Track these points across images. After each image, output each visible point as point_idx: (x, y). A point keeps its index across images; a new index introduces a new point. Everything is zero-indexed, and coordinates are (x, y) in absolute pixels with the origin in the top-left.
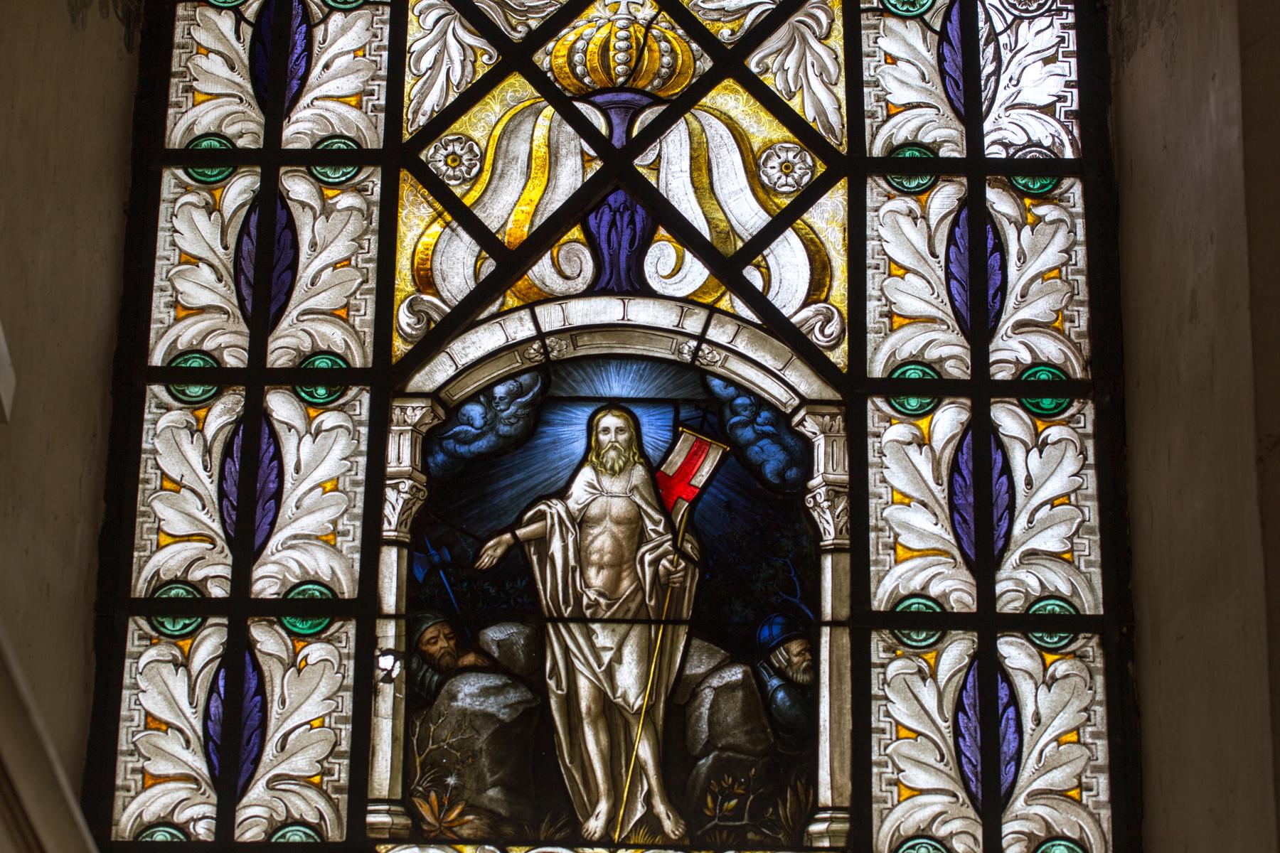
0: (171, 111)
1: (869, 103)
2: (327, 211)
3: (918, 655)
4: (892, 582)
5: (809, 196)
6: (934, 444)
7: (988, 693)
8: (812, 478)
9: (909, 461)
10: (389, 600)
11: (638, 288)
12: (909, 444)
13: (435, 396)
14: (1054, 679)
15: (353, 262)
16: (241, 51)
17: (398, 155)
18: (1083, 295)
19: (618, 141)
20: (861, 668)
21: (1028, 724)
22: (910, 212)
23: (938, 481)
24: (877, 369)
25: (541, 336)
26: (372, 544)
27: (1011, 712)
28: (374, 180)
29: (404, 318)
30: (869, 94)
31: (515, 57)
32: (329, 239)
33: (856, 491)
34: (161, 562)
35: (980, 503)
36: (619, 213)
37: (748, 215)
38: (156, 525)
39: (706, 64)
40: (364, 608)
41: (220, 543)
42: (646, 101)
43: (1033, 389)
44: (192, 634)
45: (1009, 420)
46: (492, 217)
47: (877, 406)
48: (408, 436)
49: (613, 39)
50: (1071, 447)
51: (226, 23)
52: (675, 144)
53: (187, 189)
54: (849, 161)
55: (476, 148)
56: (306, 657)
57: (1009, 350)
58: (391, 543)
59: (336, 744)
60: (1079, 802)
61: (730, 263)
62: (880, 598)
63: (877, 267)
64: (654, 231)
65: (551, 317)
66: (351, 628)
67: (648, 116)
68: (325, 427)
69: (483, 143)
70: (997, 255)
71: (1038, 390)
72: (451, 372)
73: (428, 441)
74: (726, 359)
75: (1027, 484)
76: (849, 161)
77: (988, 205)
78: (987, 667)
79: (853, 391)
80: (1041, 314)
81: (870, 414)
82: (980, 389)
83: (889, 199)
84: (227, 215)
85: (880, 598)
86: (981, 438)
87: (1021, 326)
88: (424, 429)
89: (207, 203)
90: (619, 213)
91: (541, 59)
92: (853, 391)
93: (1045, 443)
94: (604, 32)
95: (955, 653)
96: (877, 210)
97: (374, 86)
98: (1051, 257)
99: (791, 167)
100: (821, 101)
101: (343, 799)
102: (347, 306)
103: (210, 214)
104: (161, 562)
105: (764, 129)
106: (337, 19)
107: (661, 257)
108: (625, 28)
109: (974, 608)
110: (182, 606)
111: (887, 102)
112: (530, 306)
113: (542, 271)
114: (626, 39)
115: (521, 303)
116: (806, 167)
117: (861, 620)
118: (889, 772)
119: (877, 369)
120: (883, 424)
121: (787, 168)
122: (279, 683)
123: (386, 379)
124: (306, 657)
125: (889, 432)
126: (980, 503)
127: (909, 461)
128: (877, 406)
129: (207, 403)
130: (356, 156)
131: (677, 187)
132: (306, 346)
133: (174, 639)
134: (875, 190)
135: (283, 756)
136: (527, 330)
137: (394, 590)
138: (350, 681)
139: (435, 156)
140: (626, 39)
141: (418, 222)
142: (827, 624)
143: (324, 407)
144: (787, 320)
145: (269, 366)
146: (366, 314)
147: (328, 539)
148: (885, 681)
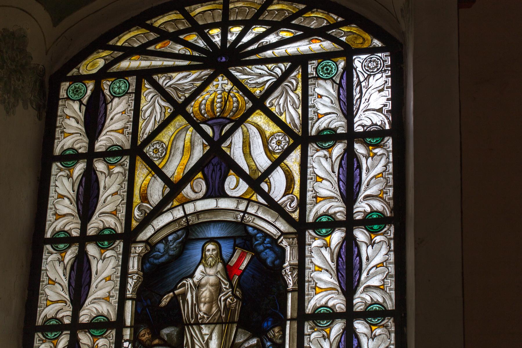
3: (323, 330)
4: (314, 302)
5: (286, 153)
7: (350, 249)
8: (285, 263)
9: (321, 254)
10: (128, 321)
12: (322, 247)
16: (81, 116)
18: (391, 183)
19: (216, 139)
20: (301, 335)
22: (325, 156)
24: (310, 218)
25: (186, 216)
28: (126, 160)
31: (179, 109)
32: (111, 183)
33: (301, 268)
34: (47, 312)
36: (216, 166)
40: (118, 324)
41: (69, 303)
44: (57, 338)
49: (216, 99)
52: (237, 138)
56: (97, 344)
62: (309, 308)
63: (312, 179)
64: (228, 172)
65: (190, 208)
66: (114, 332)
68: (107, 256)
69: (167, 143)
71: (371, 222)
73: (144, 259)
74: (254, 219)
75: (367, 260)
76: (302, 138)
77: (355, 150)
79: (301, 228)
81: (307, 237)
83: (317, 151)
84: (74, 179)
85: (309, 308)
86: (350, 242)
89: (68, 175)
90: (216, 166)
91: (189, 109)
93: (374, 243)
96: (312, 156)
98: (379, 168)
100: (292, 115)
102: (116, 210)
103: (69, 179)
105: (270, 128)
106: (116, 100)
107: (231, 181)
108: (221, 94)
109: (345, 310)
111: (318, 113)
112: (182, 205)
113: (187, 191)
115: (179, 204)
116: (286, 141)
117: (302, 317)
118: (312, 284)
119: (310, 218)
120: (312, 240)
121: (279, 143)
123: (129, 236)
124: (97, 344)
127: (321, 254)
128: (310, 233)
130: (120, 152)
131: (237, 154)
134: (311, 149)
136: (181, 214)
139: (149, 150)
140: (221, 98)
141: (142, 175)
146: (122, 214)
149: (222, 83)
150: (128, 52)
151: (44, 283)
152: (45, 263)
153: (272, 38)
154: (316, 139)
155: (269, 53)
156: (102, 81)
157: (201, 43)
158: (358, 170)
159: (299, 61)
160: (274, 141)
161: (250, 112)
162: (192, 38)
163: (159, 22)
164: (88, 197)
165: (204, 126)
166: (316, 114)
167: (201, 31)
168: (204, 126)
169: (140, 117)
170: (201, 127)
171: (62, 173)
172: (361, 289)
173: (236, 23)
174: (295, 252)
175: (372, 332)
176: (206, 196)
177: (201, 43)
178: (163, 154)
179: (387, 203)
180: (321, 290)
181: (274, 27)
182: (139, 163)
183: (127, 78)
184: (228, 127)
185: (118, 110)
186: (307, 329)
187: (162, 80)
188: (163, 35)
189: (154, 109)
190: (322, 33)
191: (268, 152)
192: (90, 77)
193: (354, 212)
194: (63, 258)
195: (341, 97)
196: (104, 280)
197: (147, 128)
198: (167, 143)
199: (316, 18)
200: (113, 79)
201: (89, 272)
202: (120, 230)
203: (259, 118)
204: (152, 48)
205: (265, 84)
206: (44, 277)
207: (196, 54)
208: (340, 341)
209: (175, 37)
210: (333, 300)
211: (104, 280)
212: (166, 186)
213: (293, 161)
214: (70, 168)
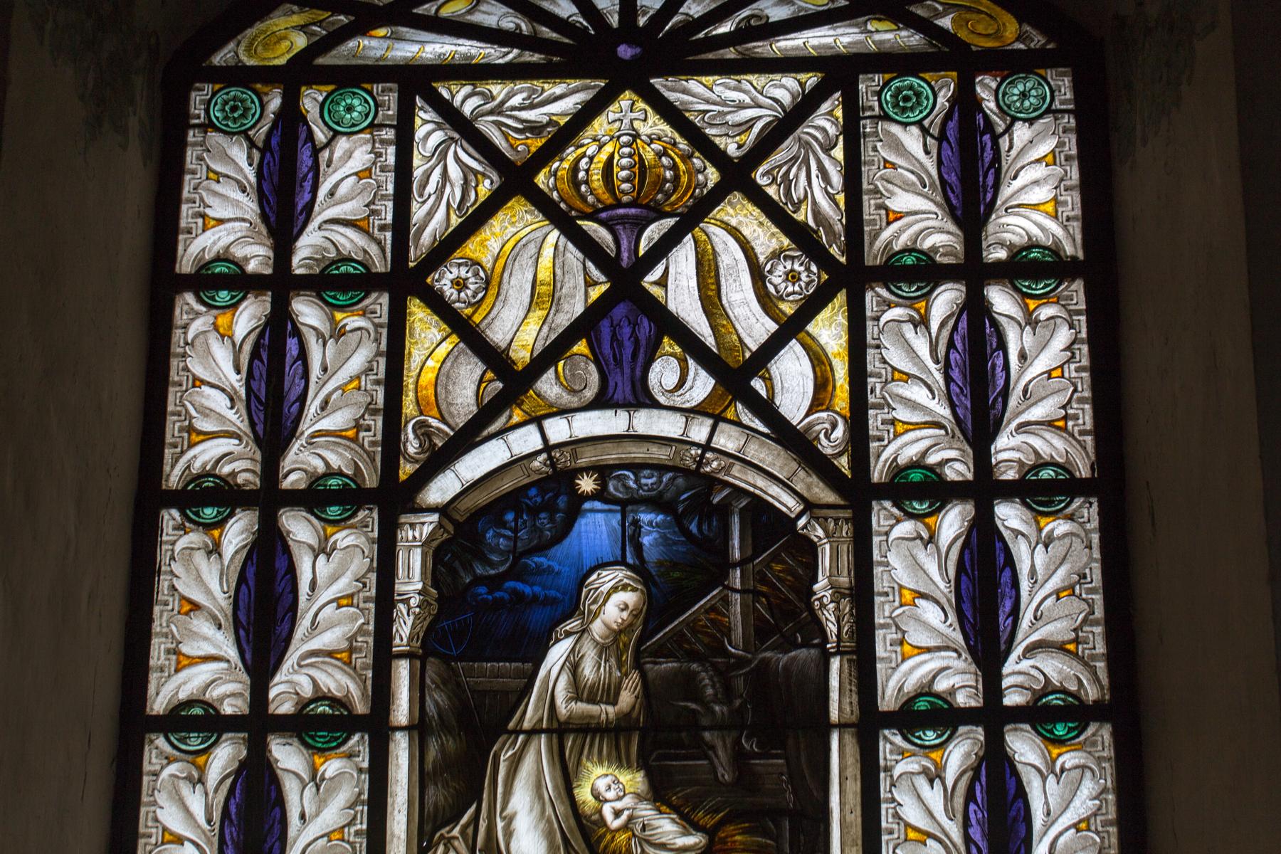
0: (181, 237)
1: (873, 364)
2: (339, 333)
4: (898, 680)
5: (812, 306)
6: (941, 544)
8: (817, 582)
9: (915, 561)
10: (402, 711)
11: (642, 399)
13: (444, 510)
15: (355, 601)
17: (405, 279)
18: (1099, 613)
20: (870, 771)
21: (1025, 585)
22: (924, 771)
24: (878, 473)
25: (548, 448)
26: (383, 656)
27: (1007, 573)
28: (381, 303)
29: (412, 446)
30: (869, 203)
31: (516, 180)
32: (339, 361)
33: (861, 593)
35: (984, 589)
36: (622, 331)
37: (755, 327)
38: (187, 423)
39: (712, 175)
40: (377, 726)
42: (652, 215)
43: (1045, 713)
44: (235, 306)
45: (1009, 515)
46: (498, 335)
47: (881, 514)
48: (419, 551)
49: (617, 157)
50: (1088, 774)
51: (239, 153)
52: (683, 261)
54: (850, 270)
55: (482, 274)
56: (335, 542)
58: (401, 656)
59: (360, 794)
60: (1065, 429)
61: (738, 377)
62: (888, 699)
64: (658, 343)
65: (558, 430)
66: (385, 299)
67: (654, 232)
71: (1052, 714)
72: (457, 488)
73: (441, 559)
74: (732, 465)
76: (850, 270)
77: (999, 523)
78: (976, 311)
79: (859, 492)
80: (1045, 415)
82: (974, 272)
85: (888, 699)
87: (1023, 427)
88: (435, 544)
90: (622, 232)
92: (859, 492)
94: (608, 149)
95: (945, 300)
97: (368, 421)
99: (794, 278)
100: (819, 196)
105: (766, 238)
106: (342, 144)
107: (663, 374)
108: (629, 145)
109: (970, 476)
111: (887, 209)
112: (538, 421)
113: (548, 386)
114: (630, 156)
115: (528, 418)
116: (810, 275)
117: (869, 724)
120: (895, 757)
122: (295, 798)
123: (393, 498)
124: (335, 542)
125: (894, 531)
126: (984, 589)
127: (915, 561)
128: (890, 741)
129: (220, 524)
131: (683, 300)
132: (321, 467)
133: (208, 527)
135: (326, 377)
136: (535, 442)
137: (405, 780)
138: (384, 346)
139: (444, 280)
140: (630, 156)
141: (427, 337)
142: (835, 726)
144: (794, 427)
148: (893, 785)
149: (627, 110)
151: (153, 840)
152: (169, 553)
154: (892, 319)
156: (303, 89)
160: (780, 270)
164: (265, 609)
165: (588, 225)
166: (883, 212)
168: (588, 225)
169: (416, 152)
170: (580, 227)
171: (173, 769)
172: (1018, 651)
174: (846, 559)
175: (1040, 530)
176: (601, 402)
178: (480, 295)
179: (1079, 442)
180: (916, 651)
182: (418, 313)
183: (367, 86)
184: (654, 232)
185: (349, 172)
186: (885, 751)
189: (446, 178)
191: (767, 301)
192: (269, 75)
193: (1004, 686)
194: (202, 770)
195: (971, 831)
196: (335, 604)
197: (432, 219)
198: (488, 266)
200: (330, 88)
201: (277, 810)
202: (380, 266)
205: (751, 127)
206: (154, 760)
208: (955, 328)
210: (948, 677)
211: (335, 604)
212: (490, 375)
213: (829, 329)
214: (198, 758)
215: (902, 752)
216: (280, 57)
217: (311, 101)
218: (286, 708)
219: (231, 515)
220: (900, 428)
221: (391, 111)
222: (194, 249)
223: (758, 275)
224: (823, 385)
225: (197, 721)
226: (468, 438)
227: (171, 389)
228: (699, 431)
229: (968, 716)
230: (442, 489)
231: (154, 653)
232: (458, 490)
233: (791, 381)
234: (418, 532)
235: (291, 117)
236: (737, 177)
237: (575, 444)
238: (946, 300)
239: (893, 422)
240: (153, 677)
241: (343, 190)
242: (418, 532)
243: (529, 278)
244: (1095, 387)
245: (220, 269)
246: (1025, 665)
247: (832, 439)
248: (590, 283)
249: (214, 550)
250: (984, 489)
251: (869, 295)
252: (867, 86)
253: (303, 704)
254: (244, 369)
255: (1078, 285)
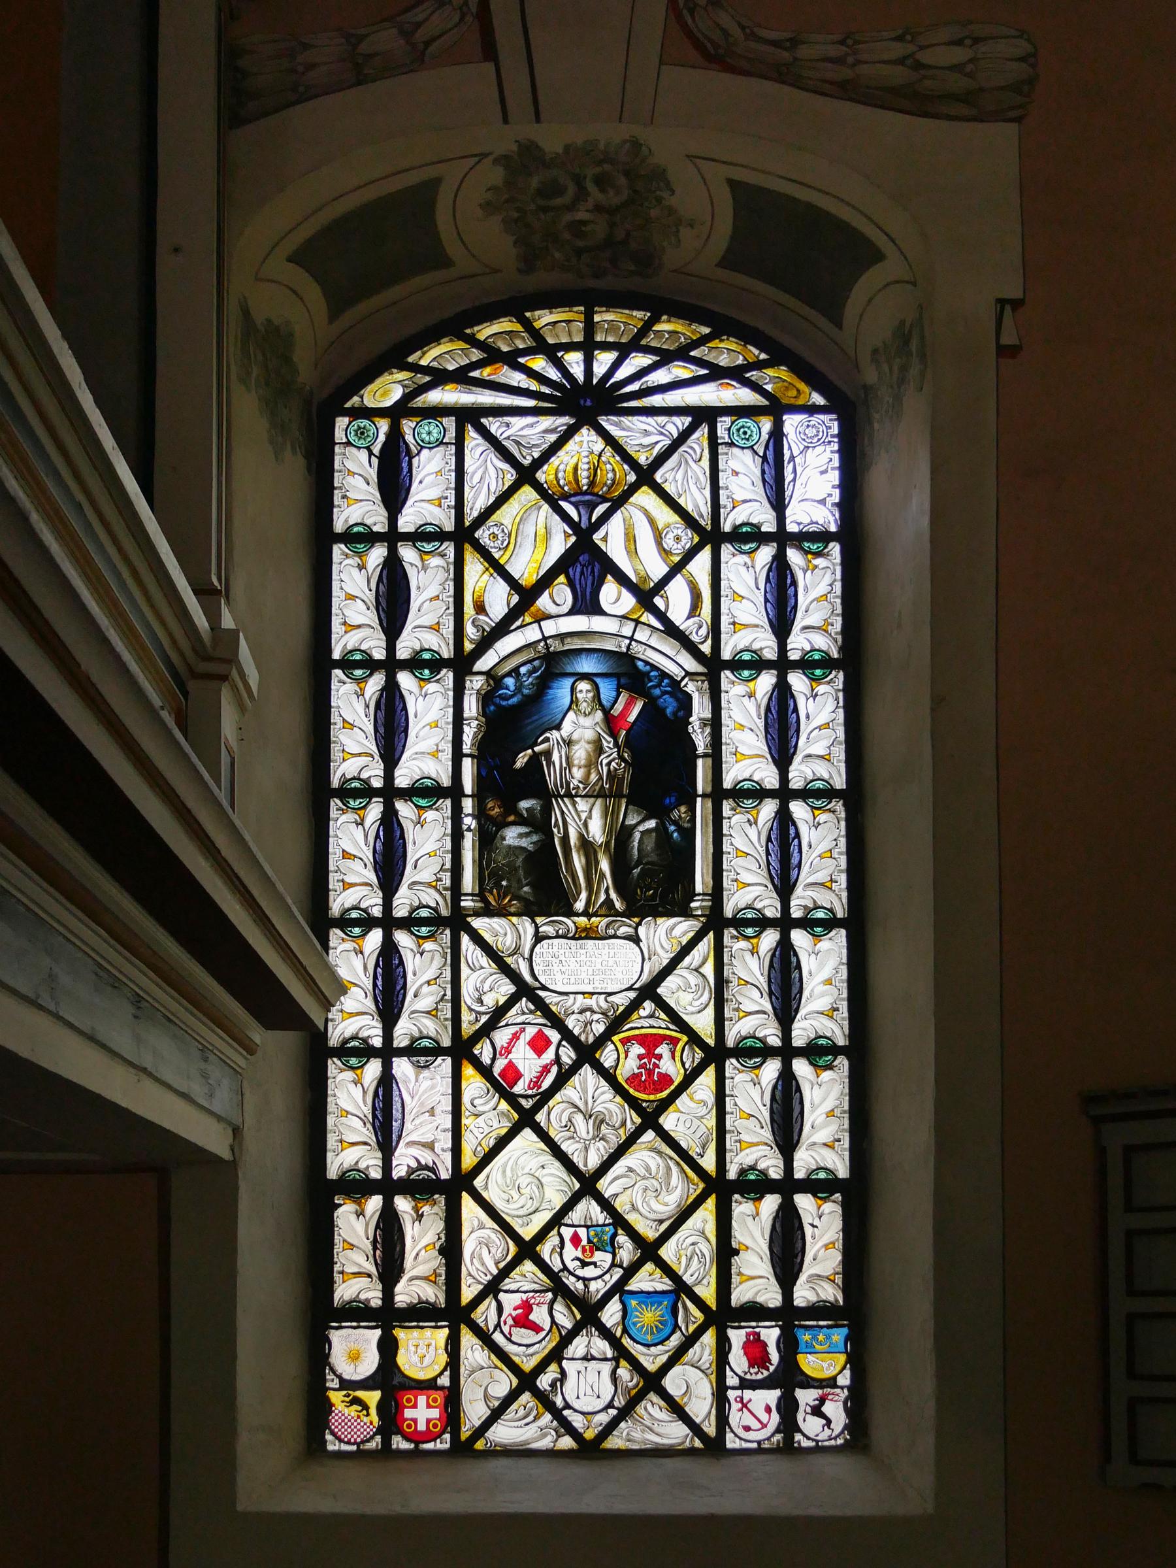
0: (335, 510)
1: (723, 500)
11: (595, 609)
13: (489, 674)
14: (819, 824)
19: (584, 525)
23: (759, 717)
25: (545, 639)
26: (458, 756)
31: (526, 475)
32: (427, 579)
33: (715, 724)
36: (585, 566)
46: (515, 570)
47: (726, 676)
52: (616, 525)
53: (342, 1071)
57: (798, 644)
59: (445, 995)
60: (826, 631)
61: (646, 595)
62: (727, 784)
65: (550, 628)
66: (448, 802)
67: (601, 509)
70: (792, 588)
73: (486, 699)
76: (711, 536)
79: (714, 667)
85: (727, 784)
90: (586, 506)
91: (540, 476)
92: (714, 667)
99: (680, 538)
101: (449, 1024)
104: (344, 1292)
105: (665, 516)
110: (357, 1313)
113: (544, 602)
116: (688, 538)
117: (718, 794)
119: (732, 1174)
123: (462, 664)
125: (732, 687)
127: (744, 704)
128: (726, 676)
130: (440, 536)
133: (353, 1068)
134: (726, 550)
139: (482, 535)
143: (428, 681)
145: (395, 1045)
147: (432, 1013)
150: (440, 377)
153: (660, 377)
155: (656, 400)
157: (553, 374)
158: (792, 588)
159: (705, 416)
161: (633, 489)
162: (539, 363)
163: (485, 332)
167: (552, 353)
171: (344, 818)
173: (606, 346)
176: (572, 612)
177: (553, 374)
181: (665, 358)
184: (601, 509)
185: (430, 473)
187: (494, 425)
188: (493, 356)
189: (486, 474)
190: (737, 374)
191: (665, 553)
199: (727, 352)
200: (418, 419)
203: (645, 497)
204: (475, 374)
207: (546, 390)
209: (511, 360)
213: (701, 565)
215: (733, 683)
216: (388, 403)
217: (407, 426)
218: (404, 1043)
219: (371, 675)
220: (744, 1145)
221: (451, 435)
222: (337, 1032)
223: (659, 538)
224: (696, 597)
225: (360, 538)
226: (502, 628)
227: (336, 474)
228: (627, 630)
229: (771, 794)
230: (486, 662)
231: (335, 498)
232: (497, 660)
233: (676, 601)
234: (476, 683)
235: (395, 435)
236: (646, 476)
237: (562, 637)
238: (770, 938)
239: (740, 1141)
240: (330, 1155)
241: (422, 734)
242: (476, 683)
243: (534, 539)
244: (841, 459)
245: (354, 915)
246: (803, 767)
247: (699, 635)
248: (567, 536)
249: (360, 823)
250: (787, 1052)
251: (727, 1063)
252: (723, 423)
253: (414, 1040)
254: (374, 589)
255: (843, 932)
